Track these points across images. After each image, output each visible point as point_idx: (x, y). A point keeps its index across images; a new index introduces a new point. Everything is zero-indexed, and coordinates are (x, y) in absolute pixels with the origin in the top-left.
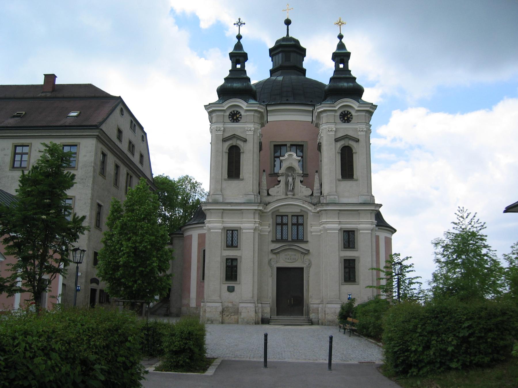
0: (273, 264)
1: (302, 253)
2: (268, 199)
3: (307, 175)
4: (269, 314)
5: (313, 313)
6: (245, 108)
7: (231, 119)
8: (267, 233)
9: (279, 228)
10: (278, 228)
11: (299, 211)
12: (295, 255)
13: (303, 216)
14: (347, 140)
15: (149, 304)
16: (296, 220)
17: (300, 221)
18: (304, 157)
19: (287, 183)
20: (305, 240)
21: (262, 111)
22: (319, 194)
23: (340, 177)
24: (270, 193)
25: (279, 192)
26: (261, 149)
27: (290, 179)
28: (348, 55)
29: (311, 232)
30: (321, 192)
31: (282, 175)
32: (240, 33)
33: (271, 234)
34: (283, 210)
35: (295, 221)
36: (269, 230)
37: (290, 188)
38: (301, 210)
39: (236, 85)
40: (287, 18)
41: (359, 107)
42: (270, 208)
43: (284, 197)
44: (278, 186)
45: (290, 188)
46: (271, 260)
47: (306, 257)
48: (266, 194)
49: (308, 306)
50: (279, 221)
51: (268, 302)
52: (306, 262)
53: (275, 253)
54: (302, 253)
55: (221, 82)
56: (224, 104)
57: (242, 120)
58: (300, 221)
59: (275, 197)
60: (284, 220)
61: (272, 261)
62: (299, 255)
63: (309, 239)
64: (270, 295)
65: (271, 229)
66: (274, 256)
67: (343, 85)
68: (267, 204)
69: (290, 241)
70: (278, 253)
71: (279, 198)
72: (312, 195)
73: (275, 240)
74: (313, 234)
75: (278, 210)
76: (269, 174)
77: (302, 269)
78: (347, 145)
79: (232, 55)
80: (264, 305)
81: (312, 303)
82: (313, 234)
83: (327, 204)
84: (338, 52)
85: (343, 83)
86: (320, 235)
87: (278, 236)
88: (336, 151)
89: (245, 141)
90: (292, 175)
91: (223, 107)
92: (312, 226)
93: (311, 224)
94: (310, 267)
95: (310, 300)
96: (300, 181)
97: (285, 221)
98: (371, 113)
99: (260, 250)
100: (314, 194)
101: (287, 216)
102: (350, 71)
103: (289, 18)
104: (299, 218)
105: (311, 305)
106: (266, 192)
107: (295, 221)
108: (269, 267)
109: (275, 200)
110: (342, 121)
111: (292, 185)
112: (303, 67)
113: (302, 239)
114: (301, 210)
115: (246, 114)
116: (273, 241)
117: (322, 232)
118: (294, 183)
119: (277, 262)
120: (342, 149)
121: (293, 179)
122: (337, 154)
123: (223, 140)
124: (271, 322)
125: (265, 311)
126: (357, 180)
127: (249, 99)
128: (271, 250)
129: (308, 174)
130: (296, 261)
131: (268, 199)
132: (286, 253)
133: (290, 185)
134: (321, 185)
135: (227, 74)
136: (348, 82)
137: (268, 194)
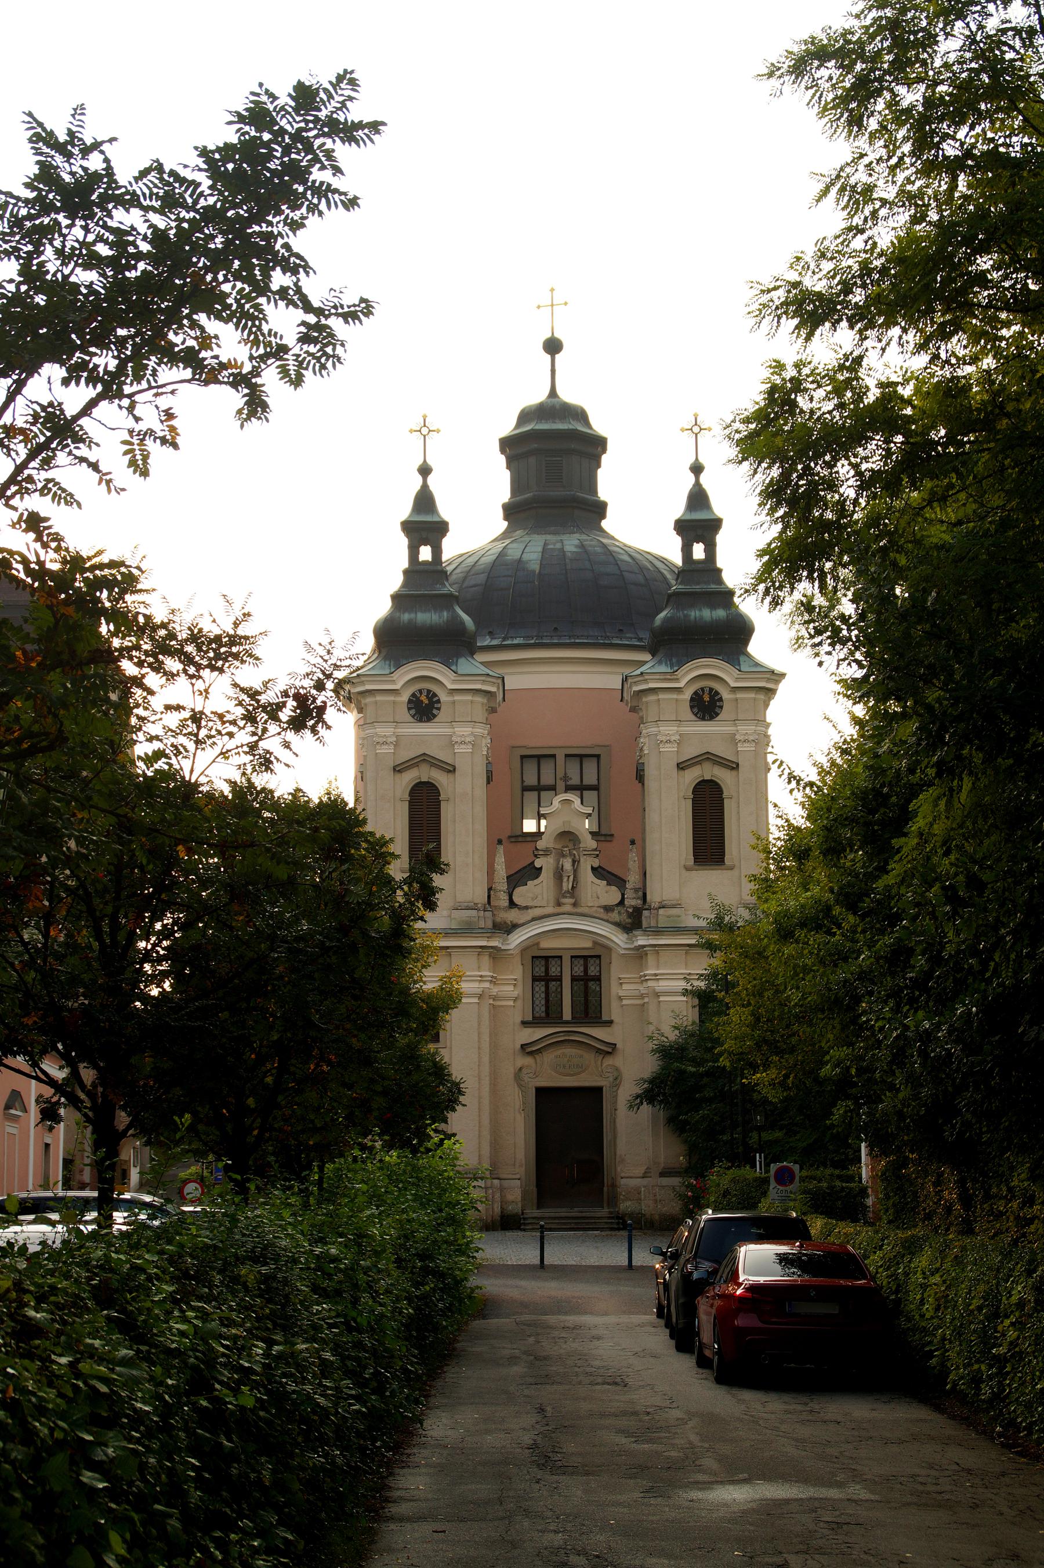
0: (526, 1079)
1: (599, 1051)
2: (513, 916)
3: (608, 838)
4: (520, 1205)
5: (628, 1199)
6: (450, 686)
7: (413, 712)
8: (511, 1003)
9: (541, 987)
10: (537, 989)
11: (588, 944)
12: (581, 1056)
13: (599, 957)
14: (707, 766)
15: (273, 1154)
16: (582, 969)
17: (593, 971)
18: (602, 788)
19: (559, 874)
20: (605, 1018)
21: (493, 689)
22: (640, 902)
23: (691, 861)
24: (515, 899)
25: (540, 897)
26: (489, 780)
27: (567, 864)
28: (715, 525)
29: (620, 998)
30: (645, 895)
31: (547, 852)
32: (428, 461)
33: (519, 1003)
34: (546, 944)
35: (579, 970)
36: (516, 993)
37: (567, 885)
38: (595, 943)
39: (426, 617)
40: (549, 335)
41: (737, 679)
42: (517, 939)
43: (550, 910)
44: (536, 882)
45: (567, 885)
46: (520, 1069)
47: (609, 1061)
48: (507, 904)
49: (614, 1186)
50: (540, 971)
51: (518, 1176)
52: (608, 1075)
53: (531, 1053)
54: (599, 1051)
55: (383, 607)
56: (395, 676)
57: (442, 715)
58: (593, 971)
59: (530, 911)
60: (553, 969)
61: (524, 1071)
62: (589, 1057)
63: (615, 1016)
64: (521, 1155)
65: (521, 994)
66: (528, 1061)
67: (701, 618)
68: (510, 928)
69: (567, 1022)
70: (539, 1051)
71: (537, 912)
72: (622, 902)
73: (530, 1019)
74: (625, 1002)
75: (538, 944)
76: (510, 837)
77: (599, 1090)
78: (707, 777)
79: (407, 527)
80: (506, 1183)
81: (623, 1175)
82: (625, 1002)
83: (658, 932)
84: (688, 517)
85: (700, 610)
86: (643, 1005)
87: (537, 1009)
88: (682, 794)
89: (451, 770)
90: (571, 854)
91: (393, 682)
92: (621, 984)
93: (620, 979)
94: (618, 1086)
95: (619, 1169)
96: (593, 868)
97: (554, 971)
98: (770, 692)
99: (494, 1046)
100: (626, 902)
101: (560, 957)
102: (720, 571)
103: (556, 335)
104: (591, 961)
105: (623, 1181)
106: (507, 897)
107: (579, 970)
108: (517, 1088)
109: (529, 918)
110: (696, 715)
111: (571, 878)
112: (599, 495)
113: (454, 668)
114: (595, 943)
115: (450, 699)
116: (525, 1023)
117: (646, 1000)
118: (575, 871)
119: (536, 1075)
120: (695, 788)
121: (574, 862)
122: (683, 802)
123: (394, 769)
124: (525, 1224)
125: (510, 1197)
126: (732, 868)
127: (458, 655)
128: (522, 1046)
129: (612, 835)
130: (583, 1071)
131: (513, 916)
132: (559, 1052)
133: (565, 879)
134: (645, 874)
135: (395, 582)
136: (713, 607)
137: (512, 904)
